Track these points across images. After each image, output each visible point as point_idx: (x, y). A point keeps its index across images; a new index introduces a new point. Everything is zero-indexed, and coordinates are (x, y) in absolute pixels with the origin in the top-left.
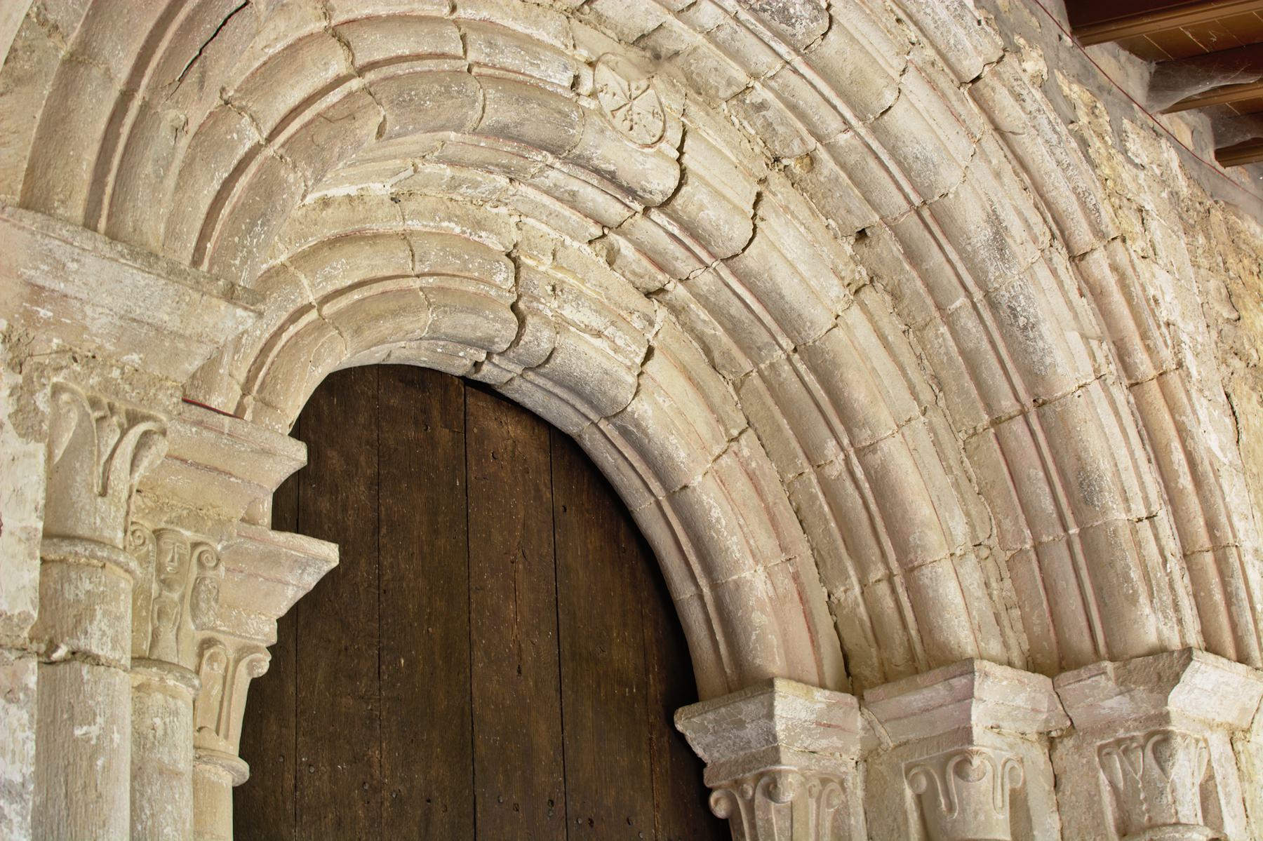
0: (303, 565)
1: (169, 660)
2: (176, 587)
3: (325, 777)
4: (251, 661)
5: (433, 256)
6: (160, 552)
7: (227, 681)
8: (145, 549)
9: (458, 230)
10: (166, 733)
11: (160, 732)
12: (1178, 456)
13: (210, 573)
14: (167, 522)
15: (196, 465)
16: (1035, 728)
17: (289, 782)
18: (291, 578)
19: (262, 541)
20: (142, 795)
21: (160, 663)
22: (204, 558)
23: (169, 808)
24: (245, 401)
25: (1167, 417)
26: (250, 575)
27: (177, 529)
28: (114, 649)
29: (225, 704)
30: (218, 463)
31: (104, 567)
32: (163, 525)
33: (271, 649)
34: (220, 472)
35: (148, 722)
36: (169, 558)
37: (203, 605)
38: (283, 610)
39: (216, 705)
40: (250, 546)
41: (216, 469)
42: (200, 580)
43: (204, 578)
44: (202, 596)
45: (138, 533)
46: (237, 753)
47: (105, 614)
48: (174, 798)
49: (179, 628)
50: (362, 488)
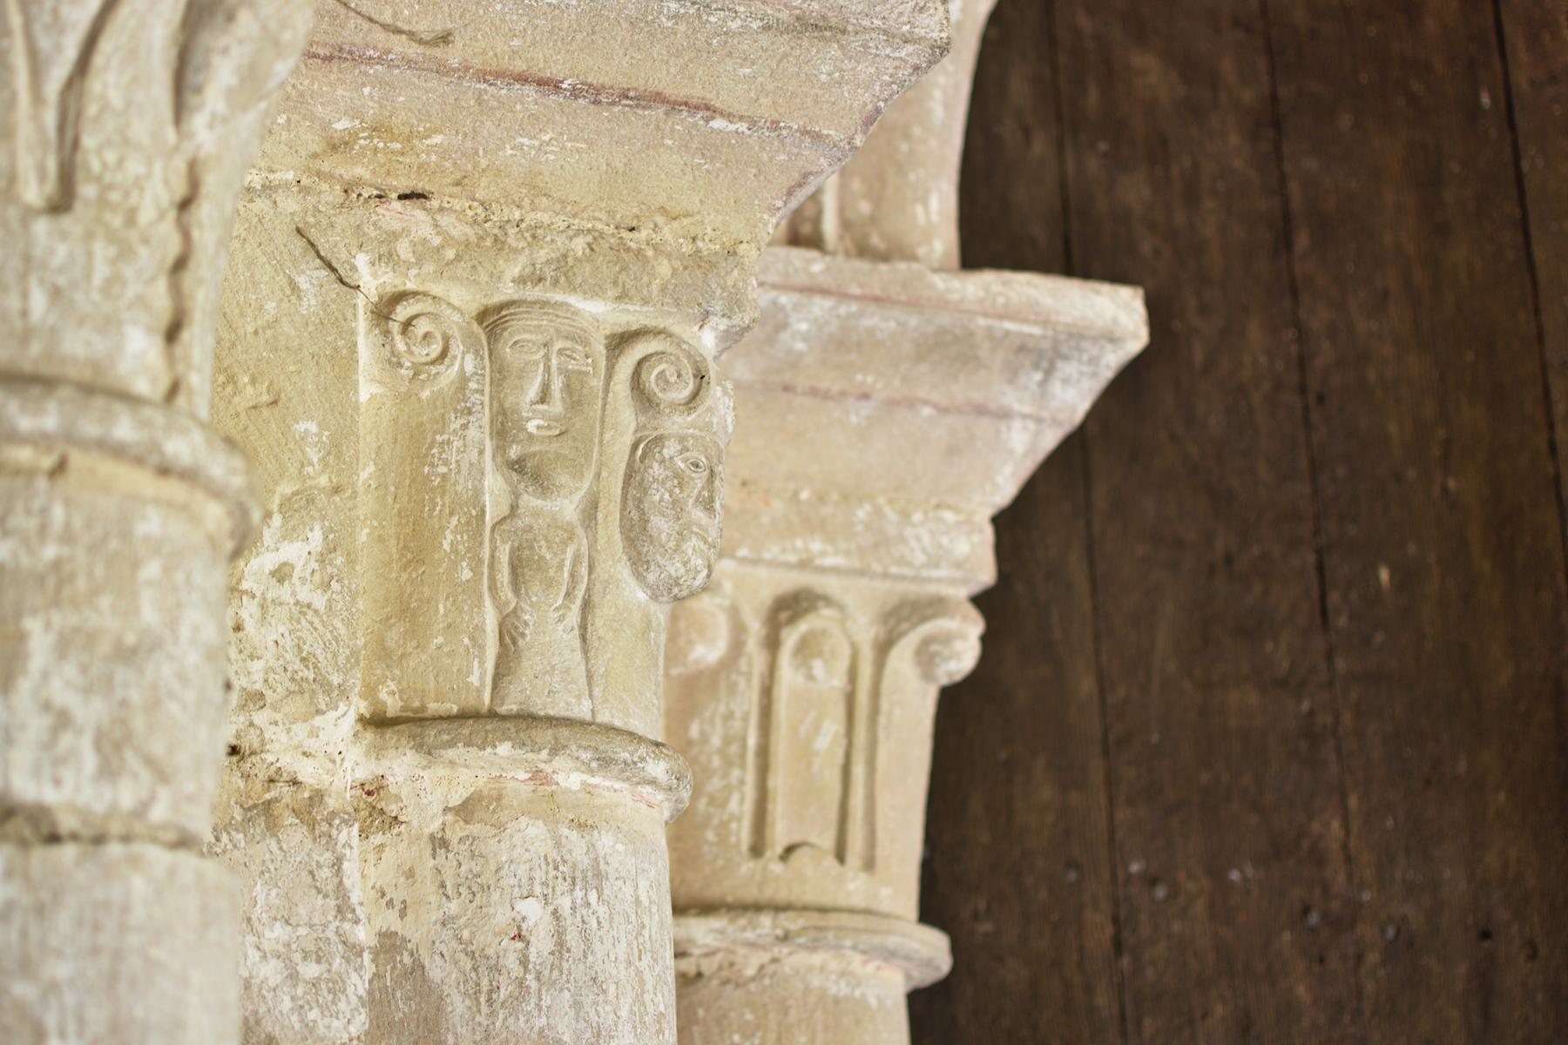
0: (1044, 355)
1: (559, 710)
2: (563, 478)
3: (1199, 907)
4: (926, 642)
6: (501, 375)
7: (859, 708)
8: (448, 375)
10: (561, 946)
11: (541, 944)
13: (676, 423)
14: (521, 281)
15: (593, 93)
17: (1098, 928)
18: (1011, 398)
19: (914, 304)
21: (527, 723)
22: (651, 379)
26: (892, 404)
27: (558, 296)
28: (108, 771)
29: (859, 771)
30: (665, 80)
31: (60, 469)
32: (508, 291)
33: (981, 601)
34: (675, 106)
35: (502, 917)
36: (533, 391)
37: (660, 525)
38: (1005, 490)
39: (833, 777)
40: (880, 322)
41: (658, 98)
42: (646, 447)
43: (659, 441)
44: (658, 495)
45: (422, 327)
47: (63, 647)
49: (587, 605)
50: (1234, 139)
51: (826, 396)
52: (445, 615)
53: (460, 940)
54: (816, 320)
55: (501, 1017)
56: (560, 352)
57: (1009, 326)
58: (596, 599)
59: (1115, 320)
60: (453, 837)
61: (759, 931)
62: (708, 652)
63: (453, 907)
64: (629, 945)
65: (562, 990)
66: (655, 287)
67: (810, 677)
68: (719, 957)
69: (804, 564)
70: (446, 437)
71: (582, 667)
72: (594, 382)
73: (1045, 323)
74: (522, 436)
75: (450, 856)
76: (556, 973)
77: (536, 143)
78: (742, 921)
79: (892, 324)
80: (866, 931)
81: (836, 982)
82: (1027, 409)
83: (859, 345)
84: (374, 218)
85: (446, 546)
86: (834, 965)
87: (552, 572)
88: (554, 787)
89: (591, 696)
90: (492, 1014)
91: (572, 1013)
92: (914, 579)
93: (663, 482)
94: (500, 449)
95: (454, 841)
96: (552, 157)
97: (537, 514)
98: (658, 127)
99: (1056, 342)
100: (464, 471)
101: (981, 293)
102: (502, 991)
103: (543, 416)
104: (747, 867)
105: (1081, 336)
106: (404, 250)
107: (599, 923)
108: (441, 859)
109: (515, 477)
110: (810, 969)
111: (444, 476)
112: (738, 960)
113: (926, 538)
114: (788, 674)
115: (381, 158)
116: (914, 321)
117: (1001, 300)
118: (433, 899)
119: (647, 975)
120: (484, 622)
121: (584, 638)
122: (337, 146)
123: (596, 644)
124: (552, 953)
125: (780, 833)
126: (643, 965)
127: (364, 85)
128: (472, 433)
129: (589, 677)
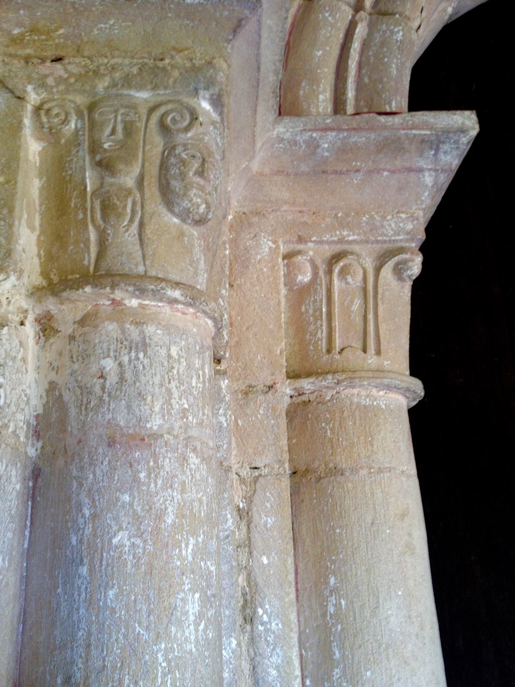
4: (397, 264)
7: (369, 294)
10: (122, 379)
11: (112, 379)
18: (422, 163)
20: (80, 485)
23: (126, 498)
24: (357, 17)
26: (370, 172)
27: (126, 92)
29: (371, 316)
35: (94, 369)
36: (108, 131)
37: (176, 184)
39: (358, 320)
42: (170, 150)
43: (174, 148)
44: (174, 171)
45: (55, 111)
46: (408, 373)
48: (136, 480)
49: (141, 225)
51: (341, 173)
52: (74, 236)
53: (77, 381)
54: (330, 142)
55: (90, 415)
56: (122, 114)
57: (414, 132)
58: (146, 221)
59: (463, 123)
60: (77, 334)
61: (327, 381)
62: (305, 277)
63: (76, 366)
64: (163, 377)
65: (121, 400)
66: (171, 81)
67: (347, 283)
68: (316, 393)
69: (341, 241)
70: (70, 158)
71: (140, 253)
72: (139, 124)
73: (431, 129)
74: (101, 150)
75: (76, 343)
76: (118, 392)
77: (108, 26)
78: (321, 378)
79: (364, 139)
80: (373, 377)
81: (365, 400)
82: (430, 167)
83: (351, 149)
84: (37, 70)
85: (73, 205)
86: (363, 393)
87: (120, 210)
88: (124, 307)
89: (145, 265)
90: (87, 415)
91: (126, 411)
92: (390, 241)
93: (175, 165)
94: (93, 158)
95: (78, 336)
96: (116, 31)
97: (111, 185)
98: (162, 8)
99: (438, 136)
100: (78, 171)
101: (401, 121)
102: (92, 403)
103: (112, 141)
104: (326, 358)
105: (449, 132)
106: (50, 81)
107: (144, 367)
108: (72, 345)
109: (99, 169)
110: (353, 395)
111: (71, 175)
112: (323, 394)
113: (393, 225)
115: (37, 44)
116: (373, 136)
117: (410, 122)
118: (68, 364)
119: (174, 390)
120: (89, 237)
121: (141, 240)
123: (147, 241)
124: (117, 383)
125: (338, 344)
126: (173, 384)
127: (19, 10)
128: (81, 153)
129: (144, 257)
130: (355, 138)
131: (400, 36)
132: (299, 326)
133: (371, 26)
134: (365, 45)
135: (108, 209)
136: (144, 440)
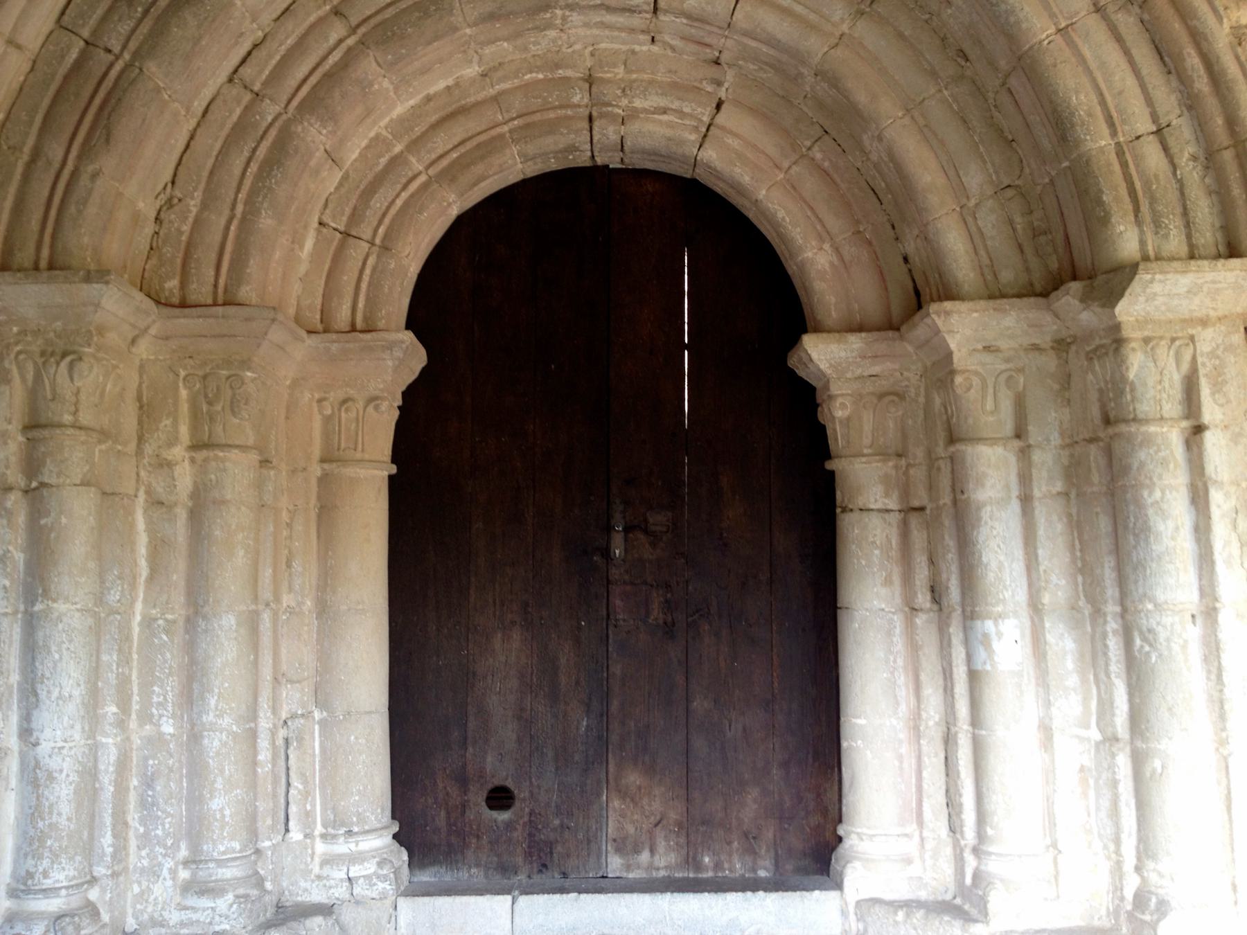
5: (518, 104)
6: (205, 387)
9: (541, 76)
12: (1193, 61)
16: (1048, 338)
25: (1177, 26)
28: (58, 477)
33: (399, 408)
42: (234, 395)
62: (329, 412)
114: (343, 414)
122: (174, 351)
125: (343, 445)
130: (351, 346)
131: (392, 266)
132: (327, 435)
133: (379, 257)
134: (374, 269)
135: (212, 419)
136: (224, 502)
